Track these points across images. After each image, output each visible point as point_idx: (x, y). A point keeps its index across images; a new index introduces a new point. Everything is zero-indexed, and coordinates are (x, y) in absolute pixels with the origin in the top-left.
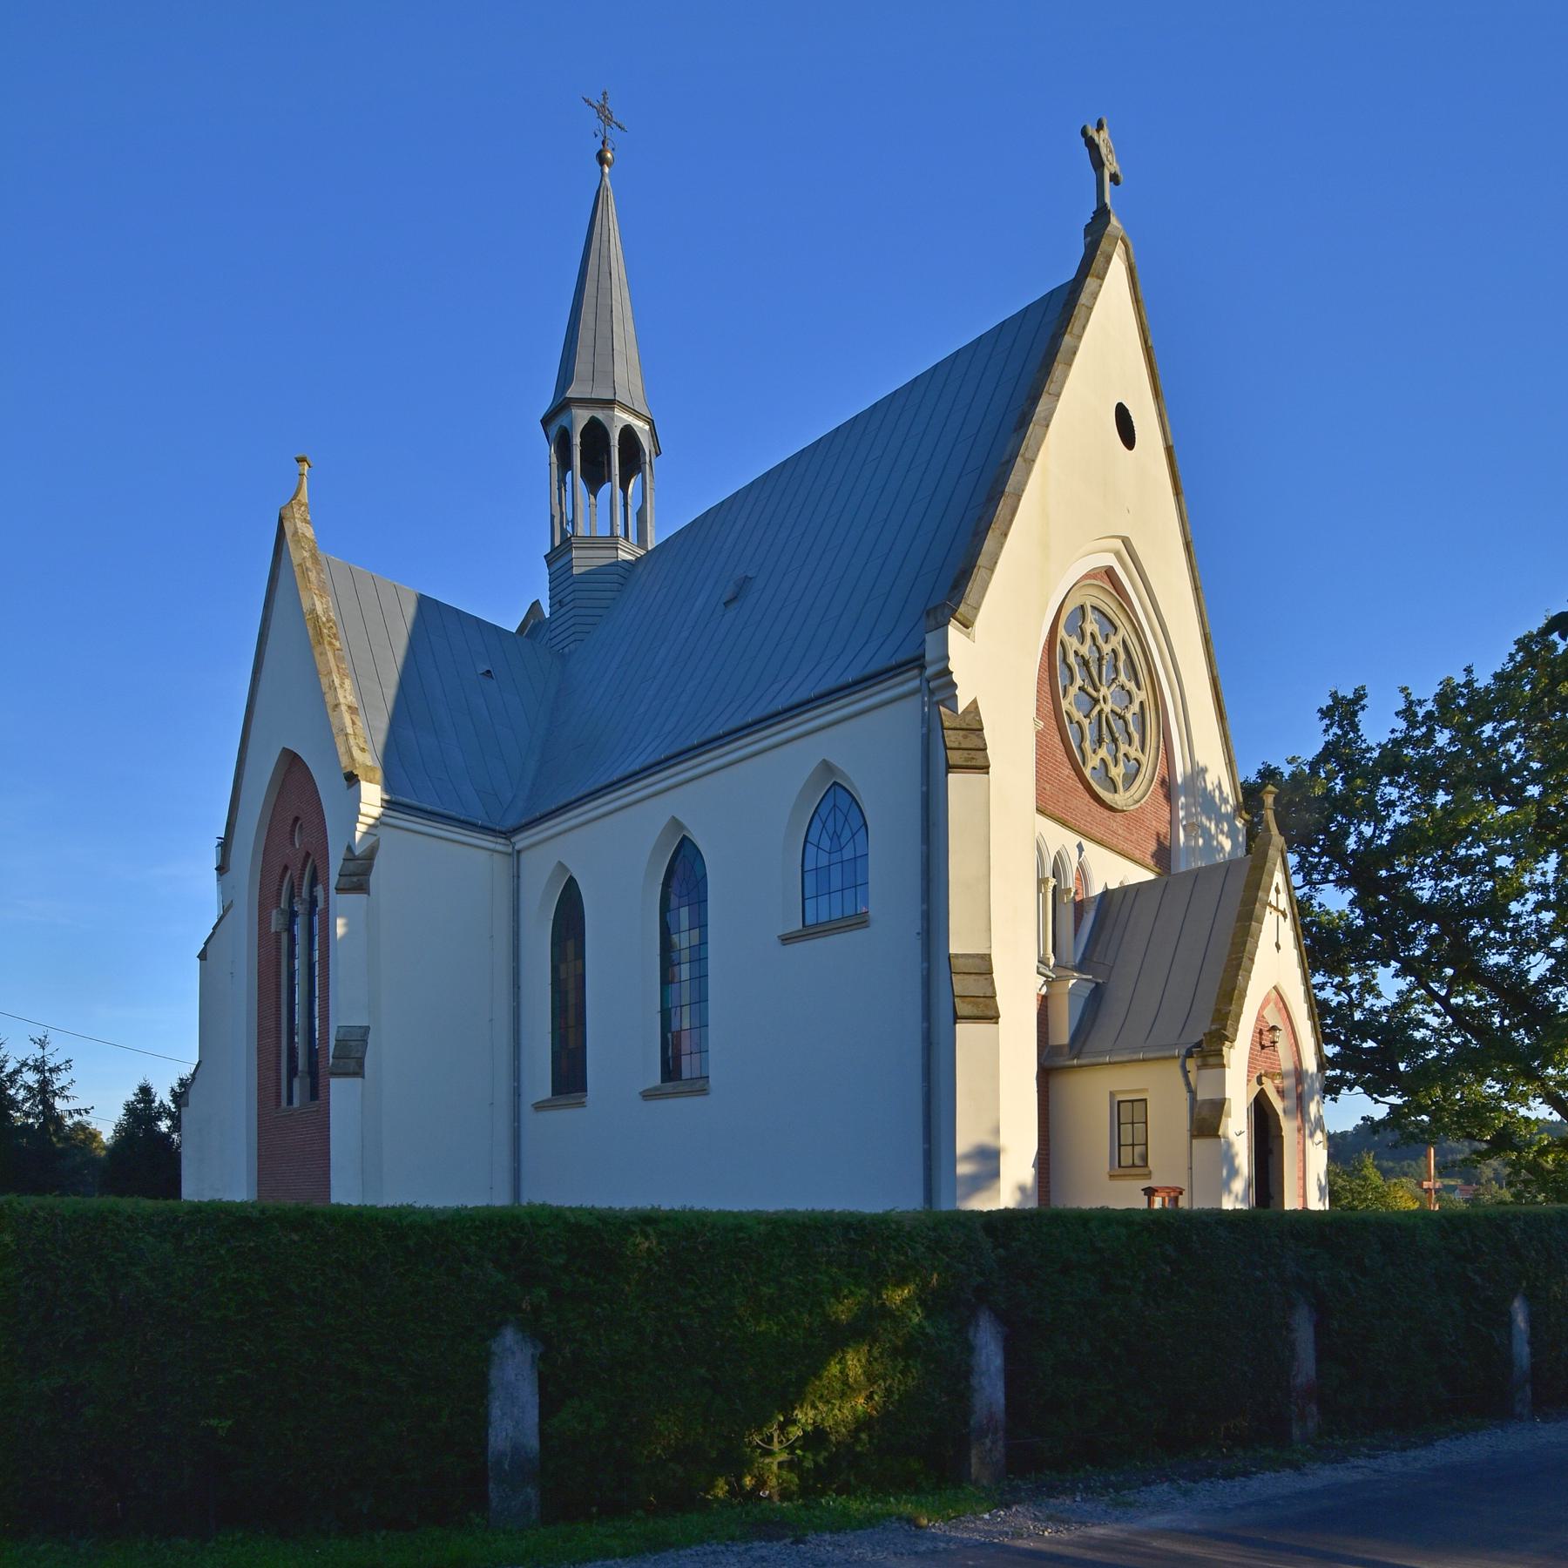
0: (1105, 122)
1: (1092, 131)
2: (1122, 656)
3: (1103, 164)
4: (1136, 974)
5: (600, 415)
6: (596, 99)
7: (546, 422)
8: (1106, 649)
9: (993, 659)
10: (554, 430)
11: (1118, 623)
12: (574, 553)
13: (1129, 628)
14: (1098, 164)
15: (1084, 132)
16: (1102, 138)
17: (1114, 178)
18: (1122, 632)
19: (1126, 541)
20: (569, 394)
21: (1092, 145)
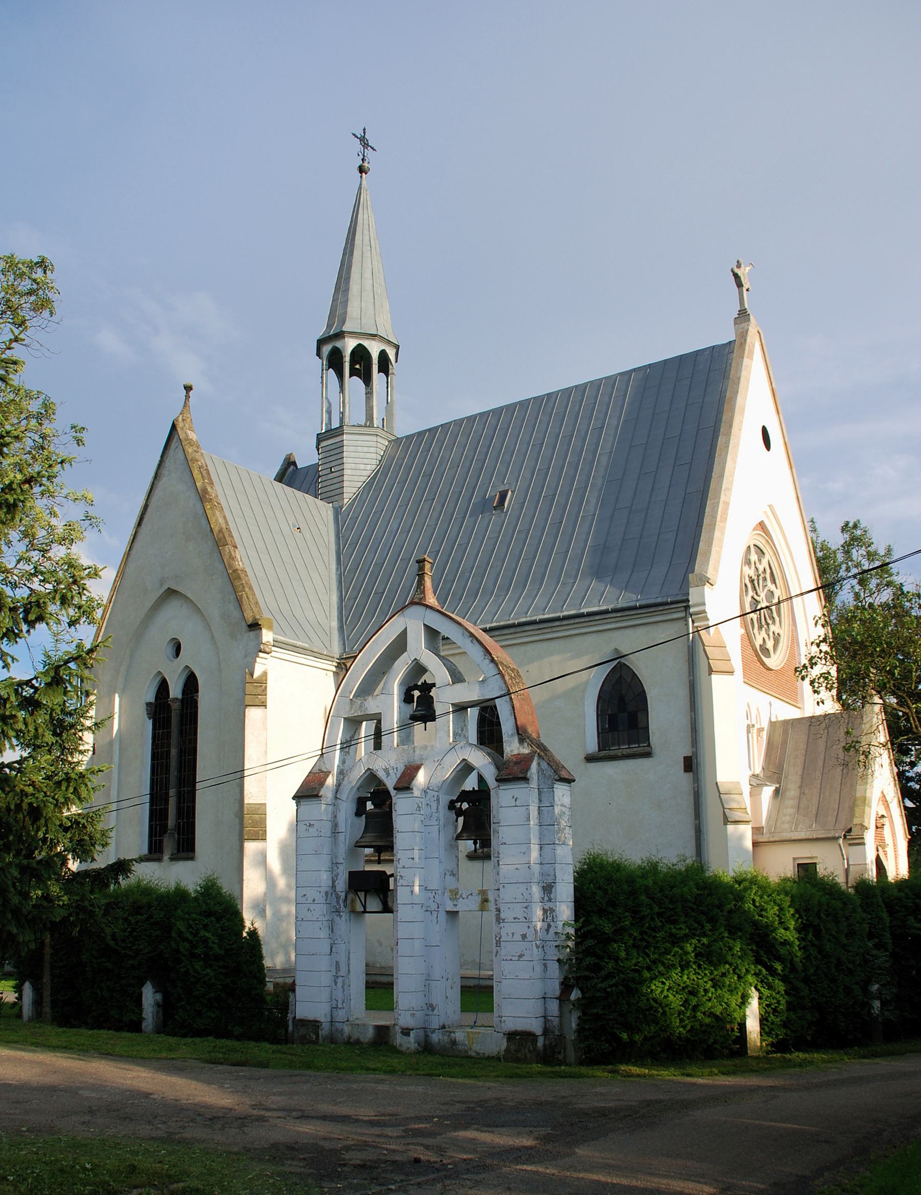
0: (741, 261)
1: (736, 270)
2: (768, 571)
3: (742, 286)
4: (814, 760)
5: (366, 343)
6: (359, 133)
7: (321, 343)
8: (761, 569)
9: (720, 597)
10: (326, 349)
11: (765, 551)
12: (345, 436)
13: (771, 553)
14: (739, 285)
15: (732, 271)
16: (743, 272)
17: (747, 290)
18: (767, 555)
19: (770, 506)
20: (344, 329)
21: (736, 276)
